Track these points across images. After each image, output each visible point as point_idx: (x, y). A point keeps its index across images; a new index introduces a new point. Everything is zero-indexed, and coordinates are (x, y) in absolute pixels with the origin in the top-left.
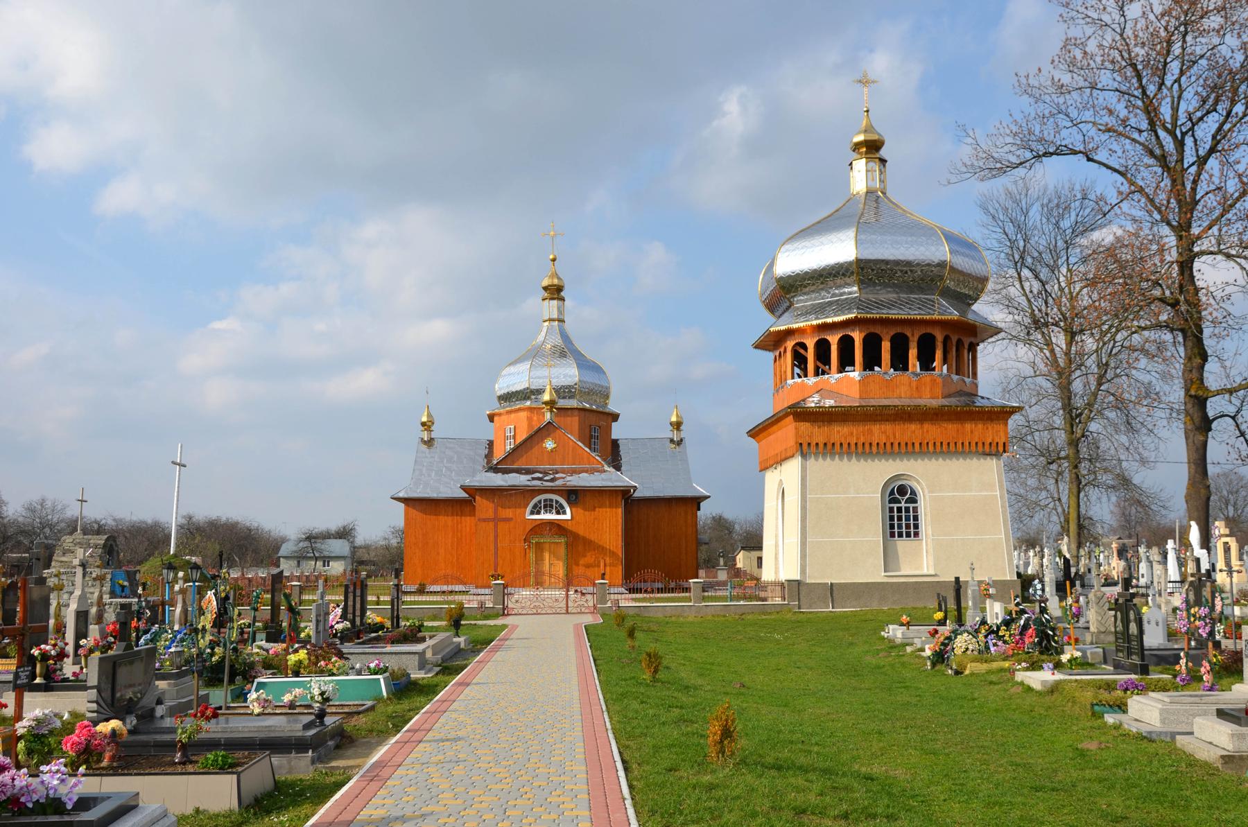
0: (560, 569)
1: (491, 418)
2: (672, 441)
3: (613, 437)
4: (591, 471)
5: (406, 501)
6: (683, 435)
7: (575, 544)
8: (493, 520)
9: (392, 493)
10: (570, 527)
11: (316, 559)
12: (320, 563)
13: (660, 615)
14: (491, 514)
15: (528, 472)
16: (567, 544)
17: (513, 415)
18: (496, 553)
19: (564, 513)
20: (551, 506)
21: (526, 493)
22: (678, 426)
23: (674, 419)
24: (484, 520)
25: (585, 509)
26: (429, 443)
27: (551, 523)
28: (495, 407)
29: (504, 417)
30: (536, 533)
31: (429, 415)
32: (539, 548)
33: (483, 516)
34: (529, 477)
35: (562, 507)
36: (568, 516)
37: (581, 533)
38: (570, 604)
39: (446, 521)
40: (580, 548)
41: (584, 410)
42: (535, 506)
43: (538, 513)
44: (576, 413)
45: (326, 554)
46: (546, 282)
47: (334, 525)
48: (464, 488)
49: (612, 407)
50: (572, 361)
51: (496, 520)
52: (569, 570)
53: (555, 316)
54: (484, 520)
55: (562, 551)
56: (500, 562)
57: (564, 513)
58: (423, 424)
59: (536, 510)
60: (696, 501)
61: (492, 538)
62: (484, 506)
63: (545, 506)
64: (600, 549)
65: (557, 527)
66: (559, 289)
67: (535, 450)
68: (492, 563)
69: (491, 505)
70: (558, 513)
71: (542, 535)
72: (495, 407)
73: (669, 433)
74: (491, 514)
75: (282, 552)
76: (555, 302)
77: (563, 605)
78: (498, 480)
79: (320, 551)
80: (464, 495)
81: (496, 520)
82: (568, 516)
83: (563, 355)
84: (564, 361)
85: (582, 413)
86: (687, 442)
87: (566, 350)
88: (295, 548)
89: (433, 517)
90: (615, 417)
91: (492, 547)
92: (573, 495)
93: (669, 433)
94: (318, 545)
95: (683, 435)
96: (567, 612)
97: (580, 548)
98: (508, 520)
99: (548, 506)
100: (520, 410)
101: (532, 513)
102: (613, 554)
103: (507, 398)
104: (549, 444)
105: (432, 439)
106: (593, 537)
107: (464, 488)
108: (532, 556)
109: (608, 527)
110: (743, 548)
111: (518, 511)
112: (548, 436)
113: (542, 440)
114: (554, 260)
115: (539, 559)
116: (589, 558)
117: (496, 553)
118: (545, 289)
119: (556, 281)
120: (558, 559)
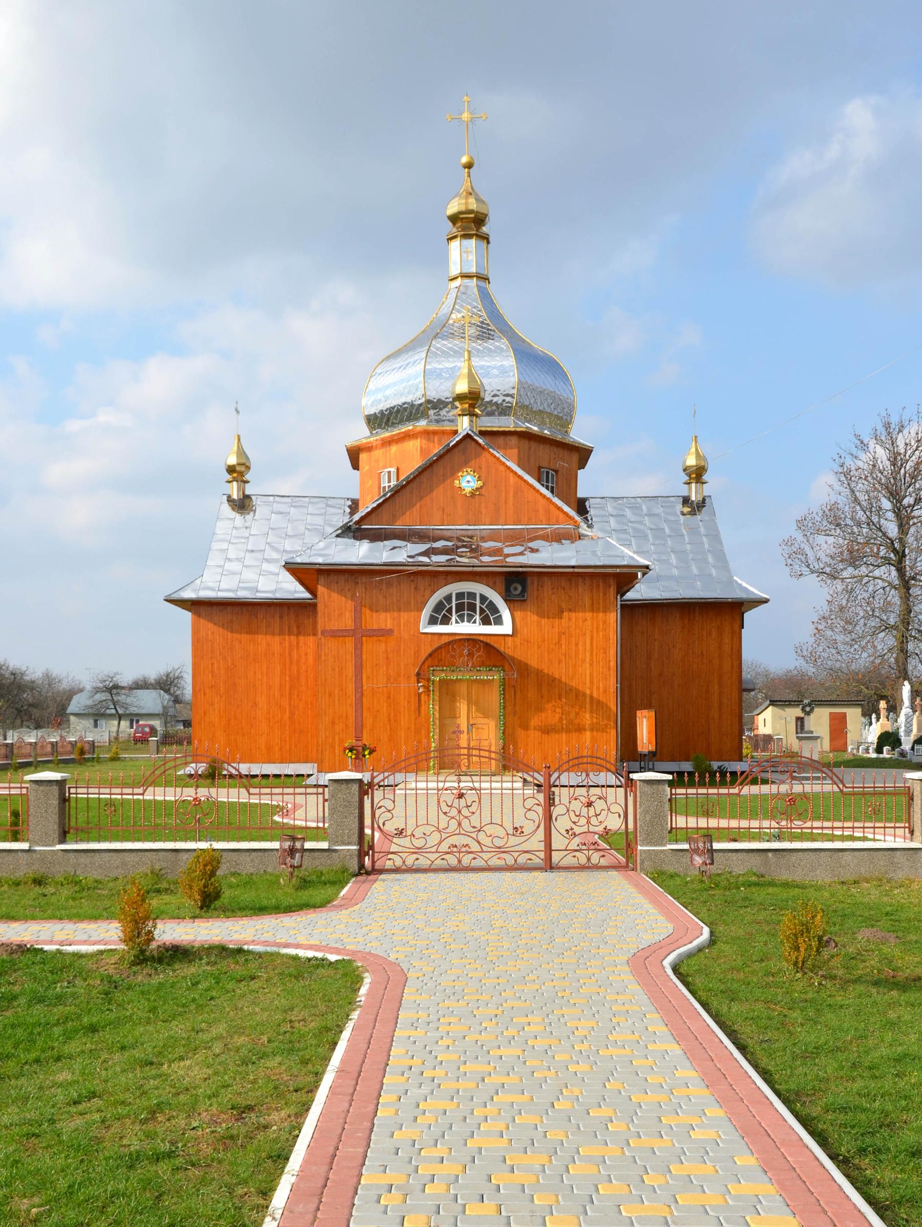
0: (489, 733)
1: (354, 455)
2: (686, 501)
3: (580, 494)
4: (558, 538)
5: (195, 606)
6: (707, 490)
7: (524, 687)
8: (352, 633)
9: (168, 591)
10: (508, 649)
11: (120, 717)
12: (125, 724)
13: (822, 876)
14: (348, 622)
15: (422, 537)
16: (504, 684)
17: (394, 448)
18: (359, 702)
19: (499, 621)
20: (472, 608)
21: (420, 578)
22: (697, 474)
23: (691, 461)
24: (334, 634)
25: (541, 615)
26: (242, 505)
27: (472, 640)
28: (360, 433)
29: (378, 453)
30: (441, 663)
31: (241, 452)
32: (448, 690)
33: (334, 625)
34: (423, 547)
35: (494, 609)
36: (506, 628)
37: (533, 662)
38: (558, 842)
39: (270, 643)
40: (532, 694)
41: (526, 436)
42: (439, 607)
43: (446, 621)
44: (514, 440)
45: (133, 710)
46: (453, 207)
47: (153, 673)
48: (298, 571)
49: (578, 434)
50: (503, 343)
51: (360, 634)
52: (508, 736)
53: (473, 270)
54: (334, 634)
55: (494, 698)
56: (368, 721)
57: (499, 621)
58: (231, 470)
59: (441, 615)
60: (732, 611)
61: (350, 670)
62: (336, 607)
63: (460, 607)
64: (576, 696)
65: (486, 651)
66: (479, 220)
67: (439, 495)
68: (351, 720)
69: (350, 604)
70: (486, 621)
71: (453, 666)
72: (360, 433)
73: (679, 486)
74: (348, 622)
75: (73, 707)
76: (473, 242)
77: (536, 843)
78: (360, 553)
79: (125, 706)
80: (298, 591)
81: (360, 634)
82: (506, 628)
83: (485, 333)
84: (489, 344)
85: (525, 443)
86: (717, 503)
87: (492, 326)
88: (89, 702)
89: (245, 637)
90: (582, 454)
91: (351, 688)
92: (517, 584)
93: (679, 486)
94: (122, 698)
95: (707, 490)
96: (549, 866)
97: (532, 694)
98: (384, 633)
99: (466, 607)
100: (407, 436)
101: (433, 621)
102: (597, 705)
103: (376, 421)
104: (468, 482)
105: (247, 497)
106: (556, 670)
107: (298, 571)
108: (432, 708)
109: (588, 651)
110: (773, 703)
111: (405, 616)
112: (466, 464)
113: (454, 473)
114: (469, 166)
115: (448, 713)
116: (551, 715)
117: (359, 702)
118: (454, 219)
119: (473, 205)
120: (486, 716)
